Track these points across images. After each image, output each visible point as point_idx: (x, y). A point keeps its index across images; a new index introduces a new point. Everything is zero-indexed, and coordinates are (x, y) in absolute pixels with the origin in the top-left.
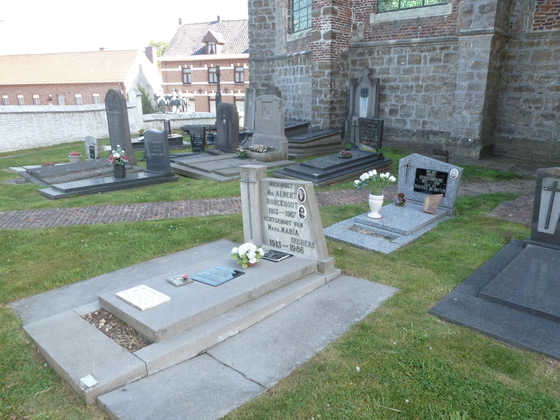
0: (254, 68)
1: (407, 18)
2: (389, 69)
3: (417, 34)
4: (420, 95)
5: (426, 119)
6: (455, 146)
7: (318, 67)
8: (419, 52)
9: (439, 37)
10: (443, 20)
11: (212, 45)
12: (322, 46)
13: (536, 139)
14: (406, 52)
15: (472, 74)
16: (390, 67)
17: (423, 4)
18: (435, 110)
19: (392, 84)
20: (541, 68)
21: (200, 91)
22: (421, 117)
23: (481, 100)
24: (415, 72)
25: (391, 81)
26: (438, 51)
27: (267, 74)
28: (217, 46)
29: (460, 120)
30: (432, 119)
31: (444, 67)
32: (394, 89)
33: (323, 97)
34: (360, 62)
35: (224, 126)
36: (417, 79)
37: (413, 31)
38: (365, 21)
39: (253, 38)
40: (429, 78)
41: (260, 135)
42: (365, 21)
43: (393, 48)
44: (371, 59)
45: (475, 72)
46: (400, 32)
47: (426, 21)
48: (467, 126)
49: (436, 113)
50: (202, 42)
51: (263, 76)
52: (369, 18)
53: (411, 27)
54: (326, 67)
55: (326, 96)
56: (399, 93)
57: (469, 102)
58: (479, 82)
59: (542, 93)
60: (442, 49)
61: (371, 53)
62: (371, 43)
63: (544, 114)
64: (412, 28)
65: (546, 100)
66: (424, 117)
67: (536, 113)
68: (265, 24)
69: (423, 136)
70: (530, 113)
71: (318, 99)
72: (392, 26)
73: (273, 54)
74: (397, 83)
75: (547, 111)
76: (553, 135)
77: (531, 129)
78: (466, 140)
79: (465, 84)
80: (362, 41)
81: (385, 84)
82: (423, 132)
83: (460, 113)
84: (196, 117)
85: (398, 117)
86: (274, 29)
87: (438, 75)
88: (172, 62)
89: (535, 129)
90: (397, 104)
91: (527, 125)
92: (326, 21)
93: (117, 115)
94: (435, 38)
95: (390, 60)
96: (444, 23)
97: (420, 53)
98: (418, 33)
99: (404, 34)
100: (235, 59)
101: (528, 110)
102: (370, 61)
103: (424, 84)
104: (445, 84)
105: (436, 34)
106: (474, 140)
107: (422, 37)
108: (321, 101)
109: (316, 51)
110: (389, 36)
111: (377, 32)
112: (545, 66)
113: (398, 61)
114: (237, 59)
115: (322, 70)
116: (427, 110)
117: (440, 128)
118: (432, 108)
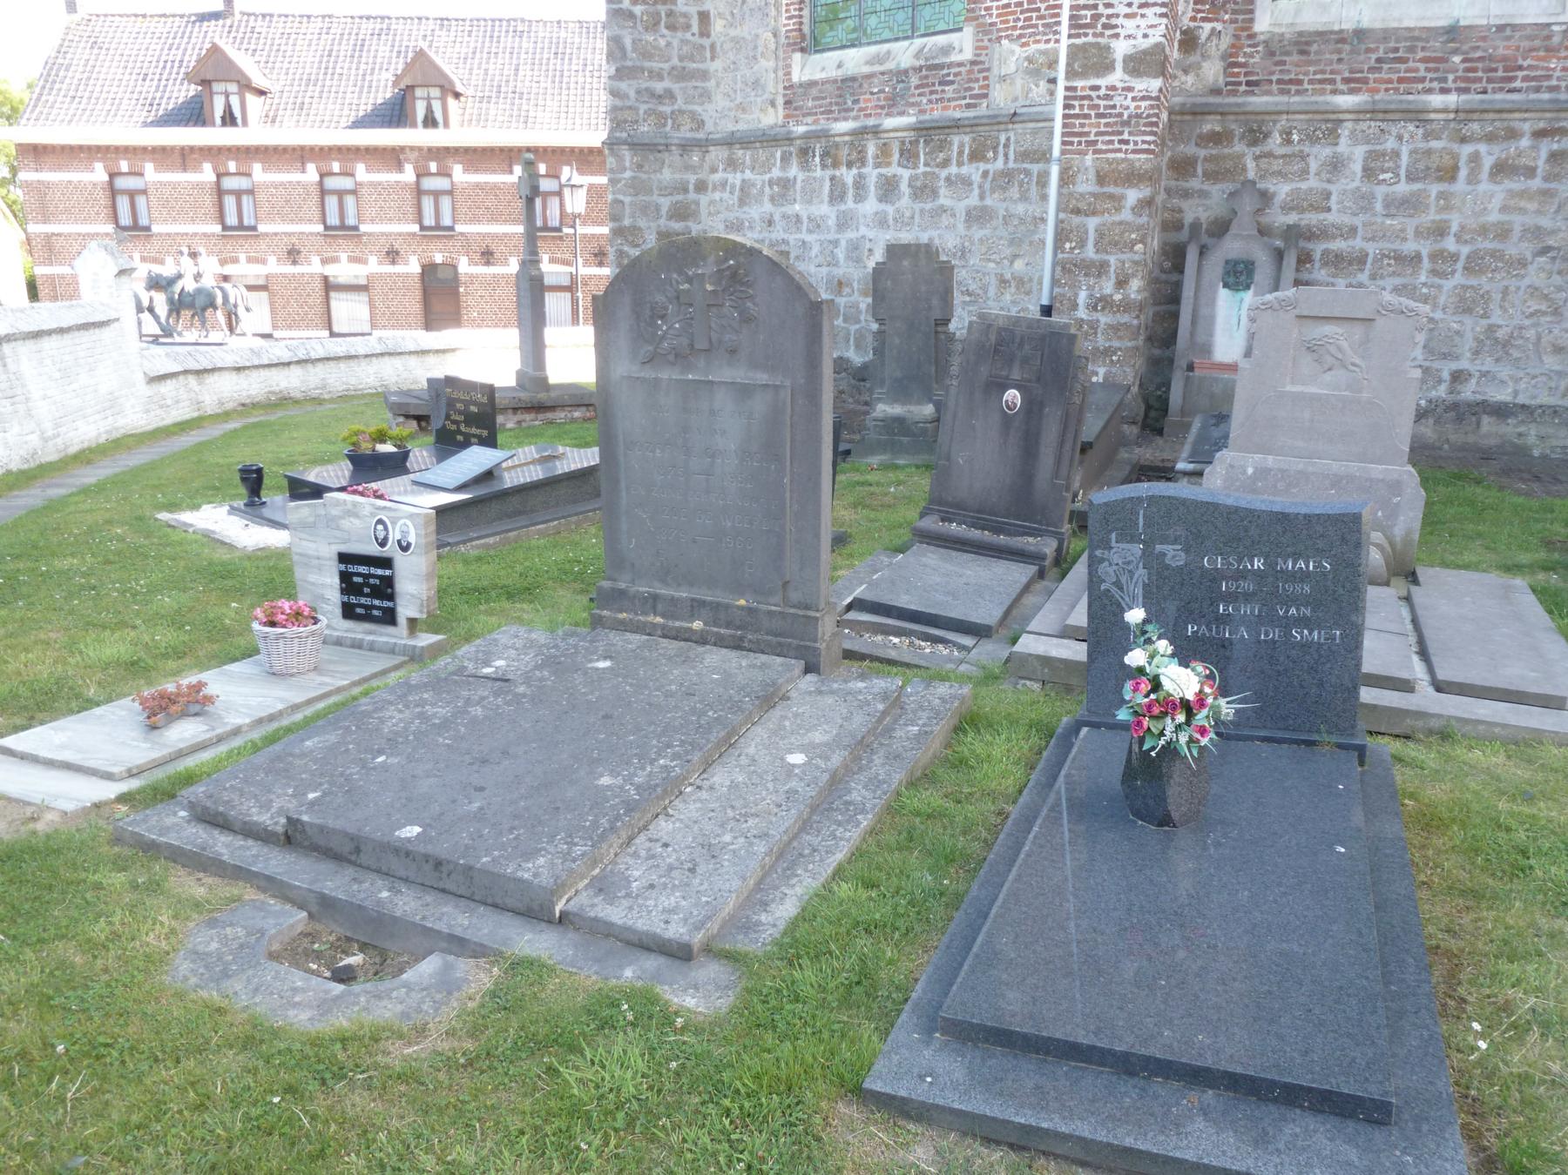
0: (628, 174)
2: (1328, 195)
3: (1445, 80)
4: (1448, 284)
5: (1464, 364)
7: (1092, 175)
8: (1451, 140)
9: (1533, 96)
10: (1549, 37)
11: (227, 95)
12: (1117, 101)
14: (1400, 138)
18: (1500, 334)
19: (1338, 245)
21: (393, 256)
22: (1445, 356)
24: (1433, 209)
25: (1334, 237)
26: (1525, 142)
27: (680, 197)
28: (250, 98)
30: (1488, 364)
31: (1546, 194)
33: (1108, 287)
34: (1211, 167)
36: (1440, 231)
37: (1428, 70)
38: (1232, 21)
39: (625, 65)
40: (1483, 230)
42: (1232, 21)
43: (1349, 125)
44: (1257, 158)
46: (1379, 70)
47: (1484, 39)
50: (189, 78)
51: (665, 203)
52: (1252, 12)
53: (1420, 55)
54: (1132, 177)
55: (1121, 283)
60: (1539, 134)
61: (1256, 136)
62: (1259, 101)
64: (1424, 60)
66: (1457, 358)
68: (670, 14)
69: (1460, 419)
71: (1082, 296)
72: (1347, 47)
73: (701, 124)
74: (1358, 243)
80: (1216, 91)
81: (1310, 246)
82: (1455, 406)
84: (314, 355)
86: (705, 33)
87: (1518, 221)
88: (63, 148)
93: (744, 391)
96: (1548, 49)
97: (1455, 147)
98: (1451, 77)
99: (1395, 77)
100: (322, 149)
102: (1251, 165)
103: (1465, 250)
104: (1545, 251)
105: (1518, 84)
107: (1466, 91)
108: (1101, 303)
109: (1087, 116)
110: (1333, 82)
111: (1283, 63)
113: (1365, 169)
114: (331, 149)
115: (1111, 189)
116: (1469, 335)
117: (1516, 393)
118: (1491, 329)
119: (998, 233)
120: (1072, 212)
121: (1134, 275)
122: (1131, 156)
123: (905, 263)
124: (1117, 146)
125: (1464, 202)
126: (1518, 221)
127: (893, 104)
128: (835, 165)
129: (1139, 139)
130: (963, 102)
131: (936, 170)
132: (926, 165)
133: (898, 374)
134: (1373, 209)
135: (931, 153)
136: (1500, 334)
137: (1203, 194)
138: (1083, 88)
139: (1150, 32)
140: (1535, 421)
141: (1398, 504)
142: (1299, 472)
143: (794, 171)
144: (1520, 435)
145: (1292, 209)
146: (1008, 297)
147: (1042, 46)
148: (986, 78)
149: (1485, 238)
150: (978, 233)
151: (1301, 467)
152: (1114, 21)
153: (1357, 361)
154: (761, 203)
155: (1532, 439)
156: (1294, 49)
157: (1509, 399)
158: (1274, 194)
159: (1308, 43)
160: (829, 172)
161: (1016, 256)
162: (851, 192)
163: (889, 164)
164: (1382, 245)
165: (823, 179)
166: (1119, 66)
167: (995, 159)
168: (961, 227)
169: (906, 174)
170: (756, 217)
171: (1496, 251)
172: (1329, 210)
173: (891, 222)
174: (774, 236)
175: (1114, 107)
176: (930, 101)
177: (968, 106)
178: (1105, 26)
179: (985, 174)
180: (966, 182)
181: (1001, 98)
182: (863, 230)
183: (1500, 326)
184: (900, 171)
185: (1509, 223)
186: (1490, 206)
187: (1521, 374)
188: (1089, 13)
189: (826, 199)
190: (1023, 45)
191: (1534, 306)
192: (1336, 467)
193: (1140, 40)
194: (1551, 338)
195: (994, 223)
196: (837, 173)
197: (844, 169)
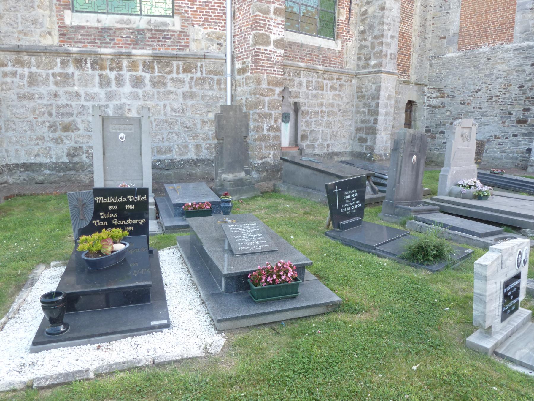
1: (311, 44)
5: (329, 142)
6: (383, 160)
7: (266, 82)
14: (313, 77)
16: (301, 91)
17: (141, 13)
26: (335, 81)
31: (339, 95)
32: (306, 113)
33: (272, 123)
35: (413, 165)
36: (321, 105)
40: (329, 105)
41: (458, 168)
53: (314, 54)
56: (308, 118)
58: (390, 110)
60: (337, 79)
71: (265, 125)
82: (329, 154)
85: (308, 143)
90: (307, 129)
92: (278, 24)
94: (332, 68)
95: (300, 84)
97: (323, 81)
103: (327, 110)
105: (332, 65)
109: (264, 60)
110: (297, 58)
115: (271, 87)
118: (333, 132)
119: (199, 102)
121: (279, 118)
122: (277, 76)
123: (231, 113)
124: (273, 72)
127: (135, 43)
128: (102, 68)
129: (279, 70)
130: (177, 47)
131: (165, 75)
132: (158, 72)
133: (230, 161)
135: (161, 67)
136: (335, 133)
138: (262, 49)
139: (280, 33)
143: (71, 69)
147: (214, 30)
148: (187, 39)
150: (190, 102)
152: (270, 27)
154: (48, 85)
156: (288, 46)
159: (291, 45)
160: (97, 73)
163: (137, 71)
164: (311, 108)
165: (93, 76)
166: (272, 43)
167: (196, 72)
168: (181, 100)
169: (147, 76)
170: (45, 92)
172: (300, 97)
173: (141, 96)
174: (59, 103)
175: (271, 58)
176: (159, 45)
177: (179, 49)
178: (268, 28)
179: (192, 78)
180: (182, 81)
181: (194, 48)
182: (123, 100)
184: (144, 74)
188: (263, 22)
190: (205, 28)
193: (277, 35)
196: (104, 73)
197: (108, 71)
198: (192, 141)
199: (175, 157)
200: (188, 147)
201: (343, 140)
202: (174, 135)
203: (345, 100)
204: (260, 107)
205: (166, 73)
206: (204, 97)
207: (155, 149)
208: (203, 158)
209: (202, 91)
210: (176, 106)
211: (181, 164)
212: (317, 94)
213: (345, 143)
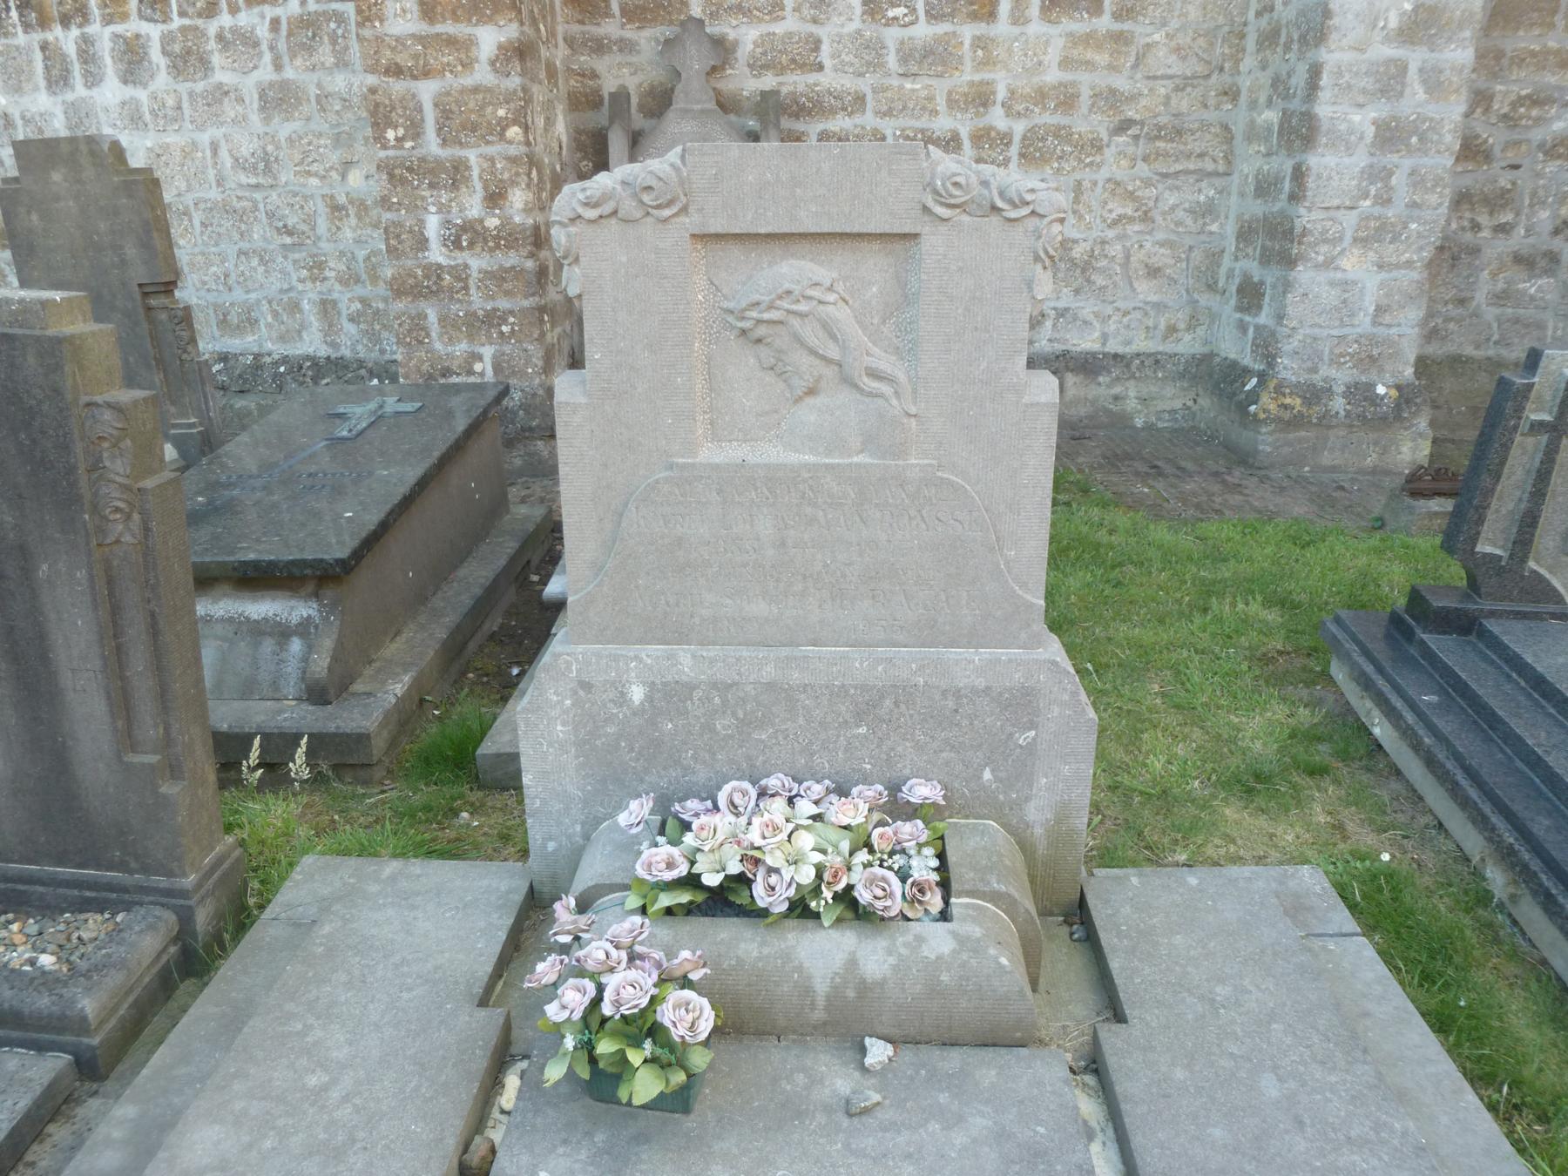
2: (817, 43)
6: (1326, 422)
13: (1491, 353)
15: (1403, 68)
16: (822, 32)
20: (1519, 61)
23: (1433, 199)
24: (968, 64)
25: (833, 112)
29: (1330, 296)
31: (1120, 38)
33: (473, 206)
36: (981, 98)
40: (1041, 96)
45: (1416, 57)
48: (1364, 323)
49: (1086, 267)
55: (495, 198)
57: (1377, 210)
58: (1432, 110)
59: (1516, 167)
63: (1524, 252)
65: (1534, 194)
67: (1496, 249)
70: (1475, 251)
74: (868, 120)
75: (1531, 240)
76: (1550, 333)
77: (1476, 314)
78: (1360, 393)
79: (1363, 120)
83: (1329, 264)
87: (1086, 82)
89: (1490, 313)
91: (1462, 302)
101: (1468, 237)
103: (1019, 128)
104: (1123, 126)
106: (1398, 388)
108: (464, 235)
112: (1533, 54)
115: (447, 28)
117: (1105, 337)
119: (313, 126)
120: (387, 72)
121: (514, 183)
123: (56, 177)
125: (1010, 51)
126: (1086, 82)
128: (44, 23)
131: (200, 22)
134: (882, 65)
136: (1078, 252)
137: (626, 46)
140: (1133, 377)
141: (1031, 748)
142: (771, 686)
144: (1116, 398)
145: (766, 67)
146: (349, 234)
149: (1044, 108)
151: (769, 672)
153: (884, 363)
155: (1131, 404)
157: (1096, 347)
158: (736, 43)
160: (37, 37)
161: (347, 165)
162: (77, 69)
163: (124, 17)
165: (29, 49)
168: (255, 118)
169: (153, 31)
171: (1060, 128)
172: (821, 67)
173: (148, 117)
179: (275, 22)
180: (250, 41)
183: (1075, 241)
185: (1073, 84)
186: (1046, 59)
187: (1109, 310)
189: (42, 83)
191: (1118, 208)
192: (858, 667)
194: (1141, 255)
195: (305, 108)
196: (50, 37)
197: (58, 30)
198: (309, 285)
199: (269, 346)
200: (301, 311)
201: (1146, 291)
202: (255, 262)
203: (1164, 61)
204: (390, 134)
205: (200, 15)
206: (323, 99)
207: (211, 311)
208: (347, 353)
209: (315, 77)
210: (247, 147)
211: (277, 376)
212: (946, 40)
213: (1159, 307)
